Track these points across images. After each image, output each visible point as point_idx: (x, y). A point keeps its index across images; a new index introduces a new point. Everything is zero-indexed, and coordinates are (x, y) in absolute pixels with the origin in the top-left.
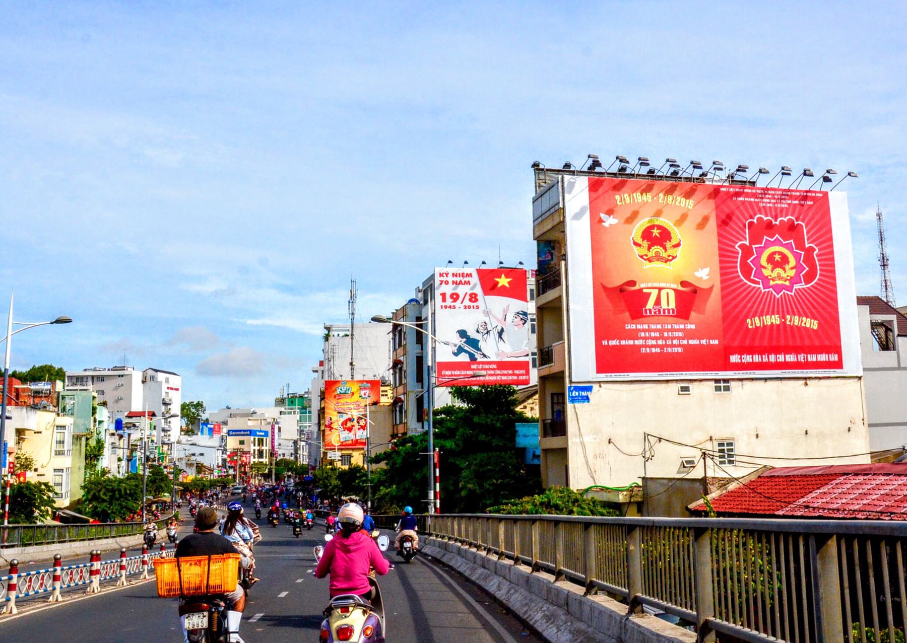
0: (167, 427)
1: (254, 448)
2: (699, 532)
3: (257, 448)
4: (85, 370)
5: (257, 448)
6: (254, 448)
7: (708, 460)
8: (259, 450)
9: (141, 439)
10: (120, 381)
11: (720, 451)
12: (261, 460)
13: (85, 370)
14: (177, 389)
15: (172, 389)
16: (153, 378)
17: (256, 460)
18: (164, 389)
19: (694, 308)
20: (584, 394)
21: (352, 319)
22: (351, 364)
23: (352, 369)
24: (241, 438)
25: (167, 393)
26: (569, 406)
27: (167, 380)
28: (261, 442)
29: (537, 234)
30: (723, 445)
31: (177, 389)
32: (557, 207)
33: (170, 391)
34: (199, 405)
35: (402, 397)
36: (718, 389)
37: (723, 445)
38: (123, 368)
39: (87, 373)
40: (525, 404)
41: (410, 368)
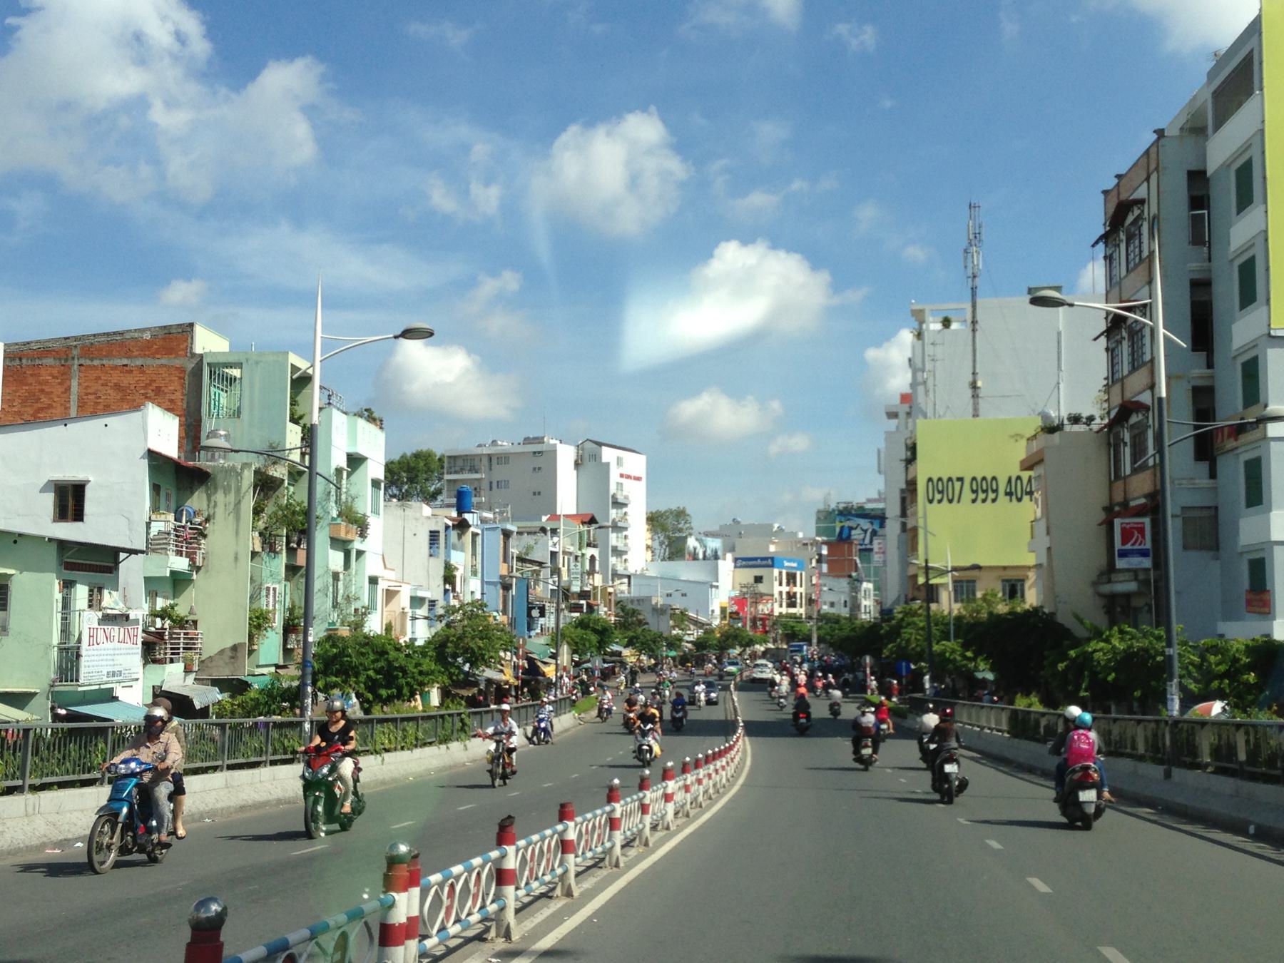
0: (621, 546)
1: (780, 589)
3: (785, 589)
4: (480, 446)
5: (785, 589)
6: (780, 589)
8: (788, 593)
9: (507, 534)
10: (538, 462)
12: (792, 610)
13: (480, 446)
14: (638, 479)
15: (629, 477)
16: (596, 457)
17: (784, 610)
18: (614, 478)
19: (1274, 504)
22: (974, 386)
23: (975, 396)
24: (758, 572)
25: (620, 485)
27: (619, 461)
28: (791, 579)
31: (638, 479)
33: (623, 480)
34: (680, 514)
38: (539, 440)
39: (479, 451)
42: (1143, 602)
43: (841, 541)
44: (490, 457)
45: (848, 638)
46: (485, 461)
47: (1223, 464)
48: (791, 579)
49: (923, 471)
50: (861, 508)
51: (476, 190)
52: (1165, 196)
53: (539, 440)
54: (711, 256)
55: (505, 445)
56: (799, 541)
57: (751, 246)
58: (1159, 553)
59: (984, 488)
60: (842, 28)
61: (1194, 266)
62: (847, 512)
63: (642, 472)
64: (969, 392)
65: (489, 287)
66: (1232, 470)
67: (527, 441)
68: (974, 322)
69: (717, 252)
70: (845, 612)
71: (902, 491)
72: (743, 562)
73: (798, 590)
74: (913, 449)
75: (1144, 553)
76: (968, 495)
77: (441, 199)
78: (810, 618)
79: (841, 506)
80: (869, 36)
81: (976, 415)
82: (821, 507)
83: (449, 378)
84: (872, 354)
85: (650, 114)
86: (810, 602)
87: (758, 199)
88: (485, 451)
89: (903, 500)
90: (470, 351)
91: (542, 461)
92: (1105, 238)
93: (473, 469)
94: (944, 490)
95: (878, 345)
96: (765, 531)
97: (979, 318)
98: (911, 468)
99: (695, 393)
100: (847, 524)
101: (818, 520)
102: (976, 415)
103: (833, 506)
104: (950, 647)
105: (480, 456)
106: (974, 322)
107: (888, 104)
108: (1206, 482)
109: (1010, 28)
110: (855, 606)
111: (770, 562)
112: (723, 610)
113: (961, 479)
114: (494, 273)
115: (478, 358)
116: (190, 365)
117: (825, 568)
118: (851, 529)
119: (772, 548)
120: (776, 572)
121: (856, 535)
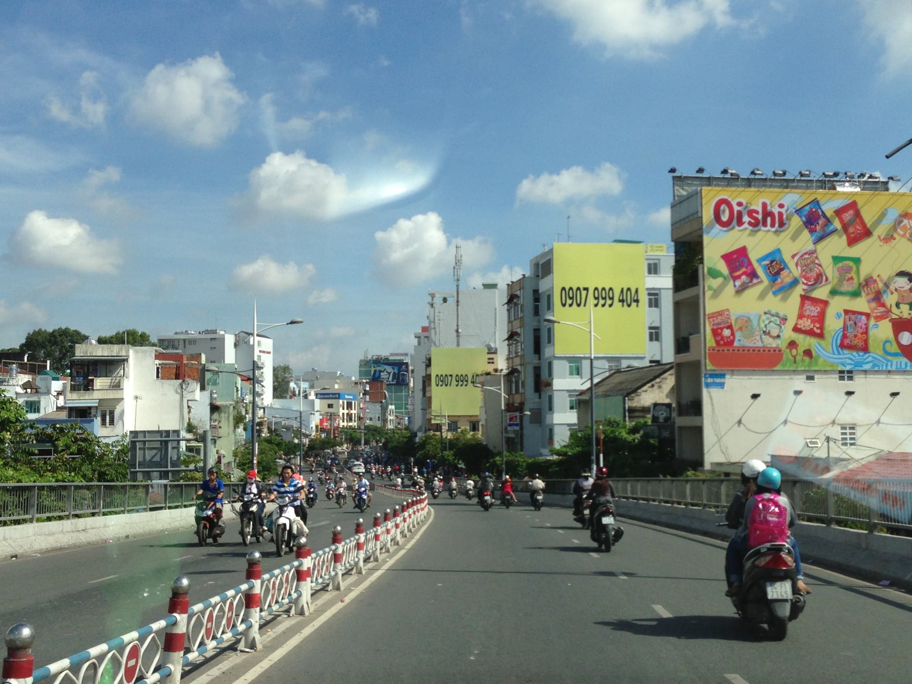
0: (260, 392)
1: (343, 411)
2: (722, 481)
3: (346, 411)
5: (346, 411)
7: (831, 443)
10: (213, 344)
11: (843, 439)
12: (350, 424)
14: (269, 353)
15: (264, 352)
17: (345, 424)
18: (257, 353)
20: (718, 380)
21: (458, 286)
22: (457, 331)
23: (458, 336)
25: (259, 357)
26: (705, 391)
27: (259, 343)
28: (349, 405)
29: (675, 237)
30: (845, 428)
31: (269, 353)
32: (696, 216)
35: (519, 368)
36: (842, 378)
37: (851, 444)
38: (215, 332)
39: (178, 337)
40: (653, 382)
41: (527, 338)
42: (514, 444)
43: (375, 380)
44: (184, 340)
45: (396, 447)
46: (181, 343)
47: (543, 394)
48: (349, 405)
49: (434, 371)
50: (387, 359)
51: (86, 105)
52: (526, 299)
53: (215, 332)
54: (264, 161)
55: (193, 333)
56: (352, 382)
57: (291, 156)
58: (521, 425)
59: (462, 380)
60: (354, 8)
61: (535, 324)
62: (378, 361)
63: (271, 350)
64: (455, 334)
65: (97, 178)
66: (545, 396)
67: (207, 332)
68: (458, 302)
69: (268, 159)
70: (379, 424)
71: (423, 377)
72: (321, 396)
73: (353, 412)
74: (430, 360)
75: (517, 425)
76: (454, 383)
77: (58, 111)
78: (359, 428)
79: (374, 358)
80: (373, 15)
81: (458, 345)
82: (362, 358)
83: (65, 242)
84: (379, 235)
85: (214, 58)
86: (360, 418)
87: (298, 124)
88: (182, 337)
89: (424, 382)
90: (81, 221)
91: (216, 345)
92: (507, 303)
93: (174, 347)
94: (444, 380)
95: (384, 229)
96: (333, 376)
97: (460, 299)
98: (428, 369)
99: (251, 258)
100: (378, 369)
101: (361, 366)
102: (458, 345)
103: (370, 357)
104: (449, 454)
105: (179, 340)
106: (458, 302)
107: (386, 63)
108: (537, 400)
109: (466, 21)
110: (385, 421)
111: (337, 396)
112: (317, 427)
113: (451, 376)
114: (100, 168)
115: (88, 227)
116: (200, 368)
117: (368, 397)
118: (380, 371)
119: (336, 386)
120: (341, 402)
121: (384, 375)
